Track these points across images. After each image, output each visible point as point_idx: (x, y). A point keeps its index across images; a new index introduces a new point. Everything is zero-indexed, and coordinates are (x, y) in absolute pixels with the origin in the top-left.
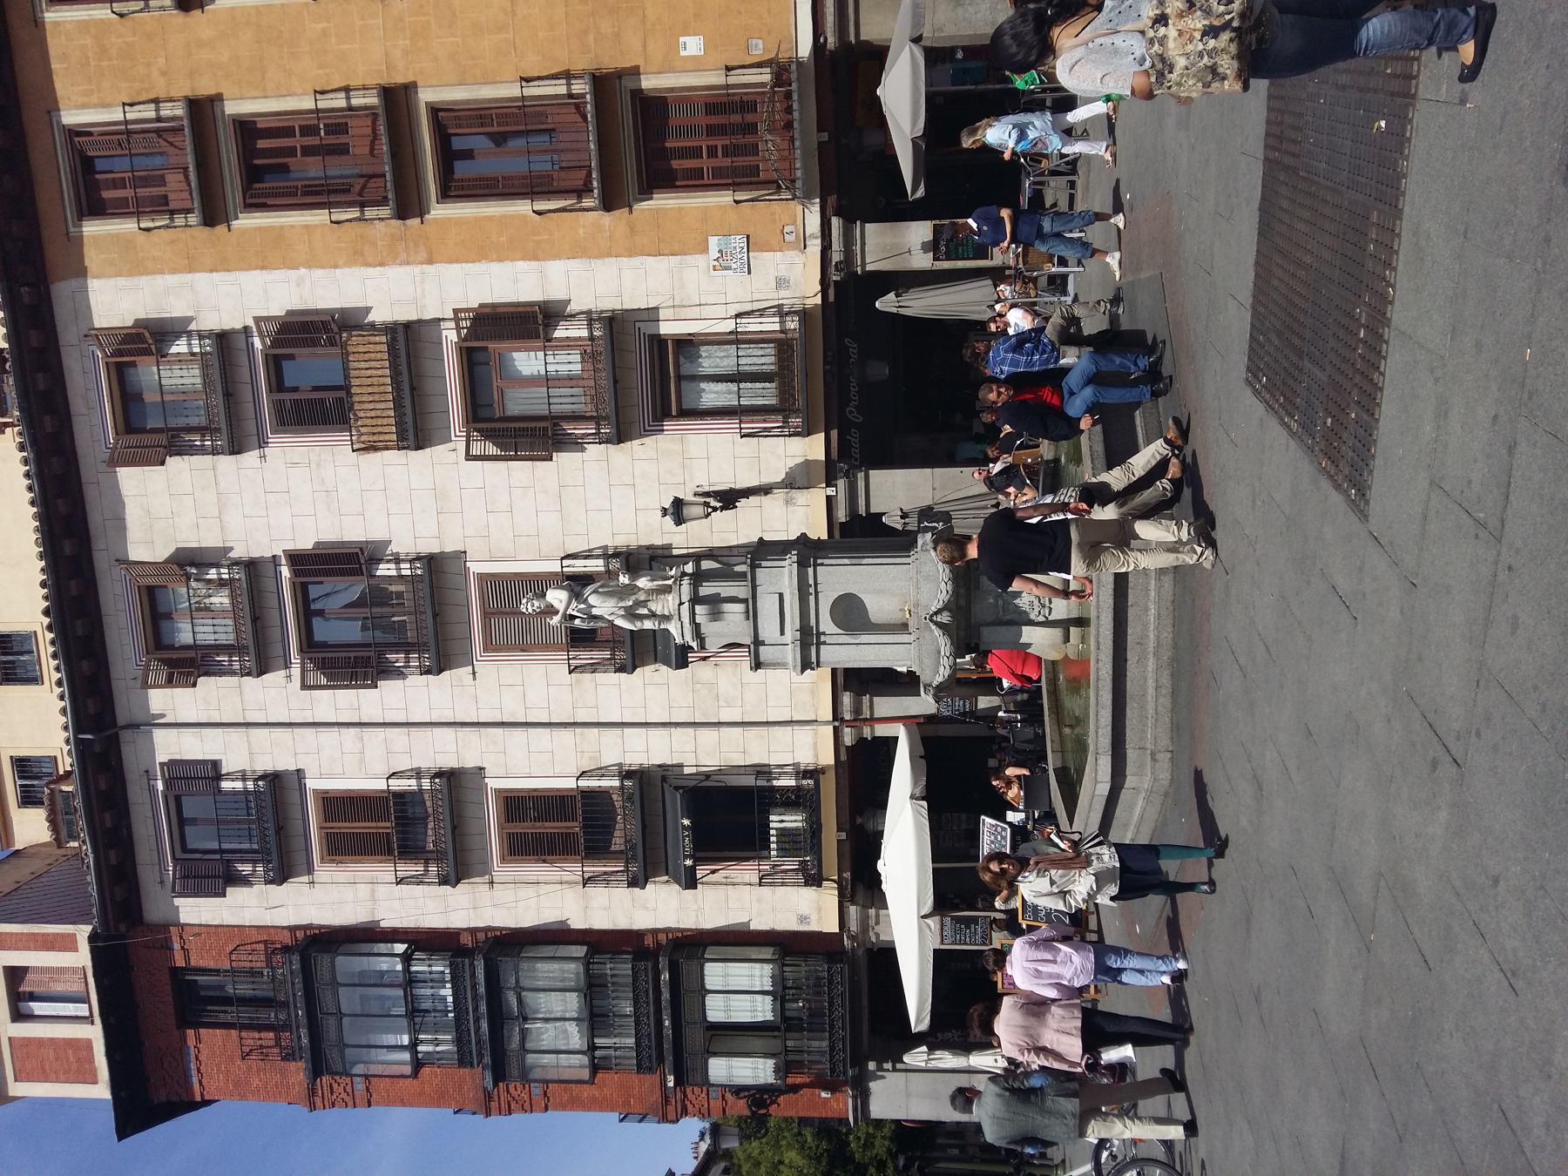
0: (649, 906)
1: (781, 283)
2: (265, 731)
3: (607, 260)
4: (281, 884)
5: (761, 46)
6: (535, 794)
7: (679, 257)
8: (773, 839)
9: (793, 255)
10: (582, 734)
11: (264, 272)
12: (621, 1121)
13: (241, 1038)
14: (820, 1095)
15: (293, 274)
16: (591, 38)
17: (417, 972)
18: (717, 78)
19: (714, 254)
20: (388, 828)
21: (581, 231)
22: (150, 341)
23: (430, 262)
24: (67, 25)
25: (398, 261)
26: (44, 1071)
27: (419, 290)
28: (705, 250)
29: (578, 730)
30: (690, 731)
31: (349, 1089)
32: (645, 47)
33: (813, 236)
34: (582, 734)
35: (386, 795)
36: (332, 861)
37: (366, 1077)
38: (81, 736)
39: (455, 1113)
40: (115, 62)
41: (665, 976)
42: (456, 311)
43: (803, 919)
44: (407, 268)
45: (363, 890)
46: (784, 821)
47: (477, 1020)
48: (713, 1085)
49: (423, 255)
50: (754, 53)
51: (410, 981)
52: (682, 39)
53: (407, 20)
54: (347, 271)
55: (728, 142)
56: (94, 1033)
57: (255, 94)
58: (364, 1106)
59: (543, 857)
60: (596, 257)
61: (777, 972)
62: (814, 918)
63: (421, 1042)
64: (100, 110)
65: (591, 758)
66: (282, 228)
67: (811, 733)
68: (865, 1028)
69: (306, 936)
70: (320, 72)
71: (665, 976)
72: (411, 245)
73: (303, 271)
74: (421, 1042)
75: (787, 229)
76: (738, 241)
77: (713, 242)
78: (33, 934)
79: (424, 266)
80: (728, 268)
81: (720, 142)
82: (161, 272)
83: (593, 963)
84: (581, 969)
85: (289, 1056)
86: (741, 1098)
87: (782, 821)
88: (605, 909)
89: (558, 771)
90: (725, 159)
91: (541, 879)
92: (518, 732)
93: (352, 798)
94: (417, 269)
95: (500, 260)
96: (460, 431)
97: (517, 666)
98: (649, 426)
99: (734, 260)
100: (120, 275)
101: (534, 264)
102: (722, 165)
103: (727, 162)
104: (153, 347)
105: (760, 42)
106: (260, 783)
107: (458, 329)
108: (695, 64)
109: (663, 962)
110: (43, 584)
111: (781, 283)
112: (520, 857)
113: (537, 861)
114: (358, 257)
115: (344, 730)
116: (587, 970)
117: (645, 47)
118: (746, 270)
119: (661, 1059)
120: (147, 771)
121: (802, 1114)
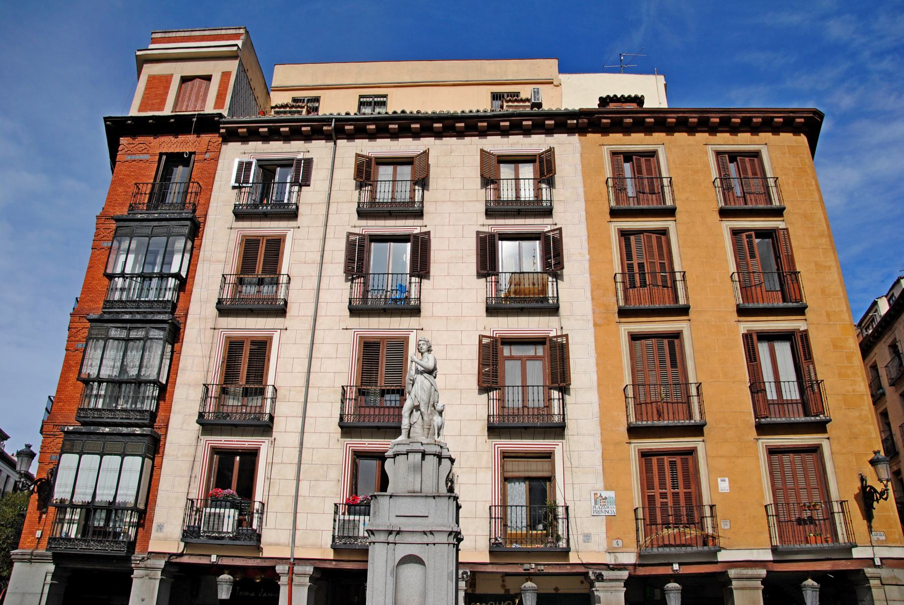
0: (185, 425)
1: (587, 537)
2: (324, 212)
3: (599, 427)
4: (234, 212)
5: (726, 528)
6: (266, 360)
7: (601, 472)
8: (218, 510)
9: (604, 546)
10: (301, 391)
11: (586, 237)
12: (49, 397)
13: (147, 184)
14: (39, 529)
15: (586, 251)
16: (724, 425)
17: (168, 281)
18: (706, 500)
19: (605, 494)
20: (258, 272)
21: (615, 413)
22: (548, 176)
23: (595, 325)
24: (706, 158)
25: (594, 307)
26: (151, 88)
27: (579, 317)
28: (607, 488)
29: (304, 389)
30: (296, 461)
31: (106, 238)
32: (721, 457)
33: (616, 558)
34: (301, 391)
35: (278, 273)
36: (242, 241)
37: (111, 248)
38: (334, 120)
39: (77, 298)
40: (691, 177)
41: (138, 431)
42: (567, 336)
43: (160, 527)
44: (591, 312)
45: (222, 257)
46: (229, 518)
47: (131, 313)
48: (60, 456)
49: (599, 321)
50: (722, 523)
51: (163, 276)
52: (727, 479)
53: (725, 324)
54: (588, 280)
55: (669, 505)
56: (167, 111)
57: (680, 242)
58: (93, 246)
59: (226, 361)
60: (600, 421)
61: (128, 506)
62: (160, 535)
63: (125, 281)
64: (667, 167)
65: (285, 396)
66: (611, 248)
67: (287, 543)
68: (79, 566)
69: (200, 223)
70: (694, 276)
71: (138, 431)
72: (604, 316)
73: (588, 257)
74: (125, 281)
75: (620, 542)
76: (612, 510)
77: (611, 494)
78: (227, 90)
79: (592, 322)
80: (596, 503)
81: (669, 500)
82: (585, 186)
83: (154, 386)
84: (151, 378)
85: (132, 208)
86: (47, 475)
87: (229, 517)
88: (187, 397)
89: (279, 375)
90: (660, 504)
91: (212, 359)
92: (305, 352)
93: (278, 255)
94: (591, 317)
95: (597, 365)
96: (496, 334)
97: (349, 355)
98: (498, 448)
99: (601, 507)
100: (582, 167)
101: (595, 384)
102: (656, 501)
103: (658, 505)
104: (544, 178)
105: (728, 527)
106: (294, 207)
107: (557, 337)
108: (713, 487)
109: (147, 430)
110: (418, 112)
111: (587, 537)
112: (228, 348)
113: (224, 358)
114: (595, 286)
115: (319, 254)
116: (150, 382)
117: (721, 457)
118: (595, 514)
119: (84, 424)
120: (309, 152)
121: (28, 516)
